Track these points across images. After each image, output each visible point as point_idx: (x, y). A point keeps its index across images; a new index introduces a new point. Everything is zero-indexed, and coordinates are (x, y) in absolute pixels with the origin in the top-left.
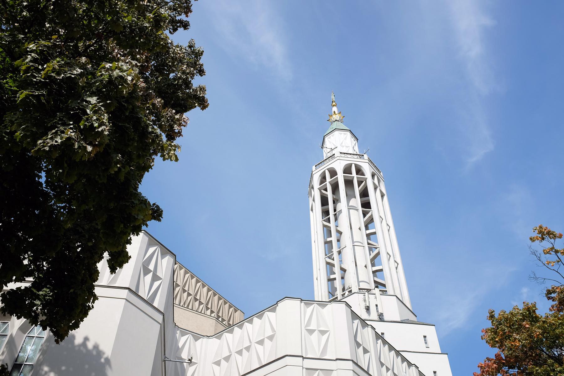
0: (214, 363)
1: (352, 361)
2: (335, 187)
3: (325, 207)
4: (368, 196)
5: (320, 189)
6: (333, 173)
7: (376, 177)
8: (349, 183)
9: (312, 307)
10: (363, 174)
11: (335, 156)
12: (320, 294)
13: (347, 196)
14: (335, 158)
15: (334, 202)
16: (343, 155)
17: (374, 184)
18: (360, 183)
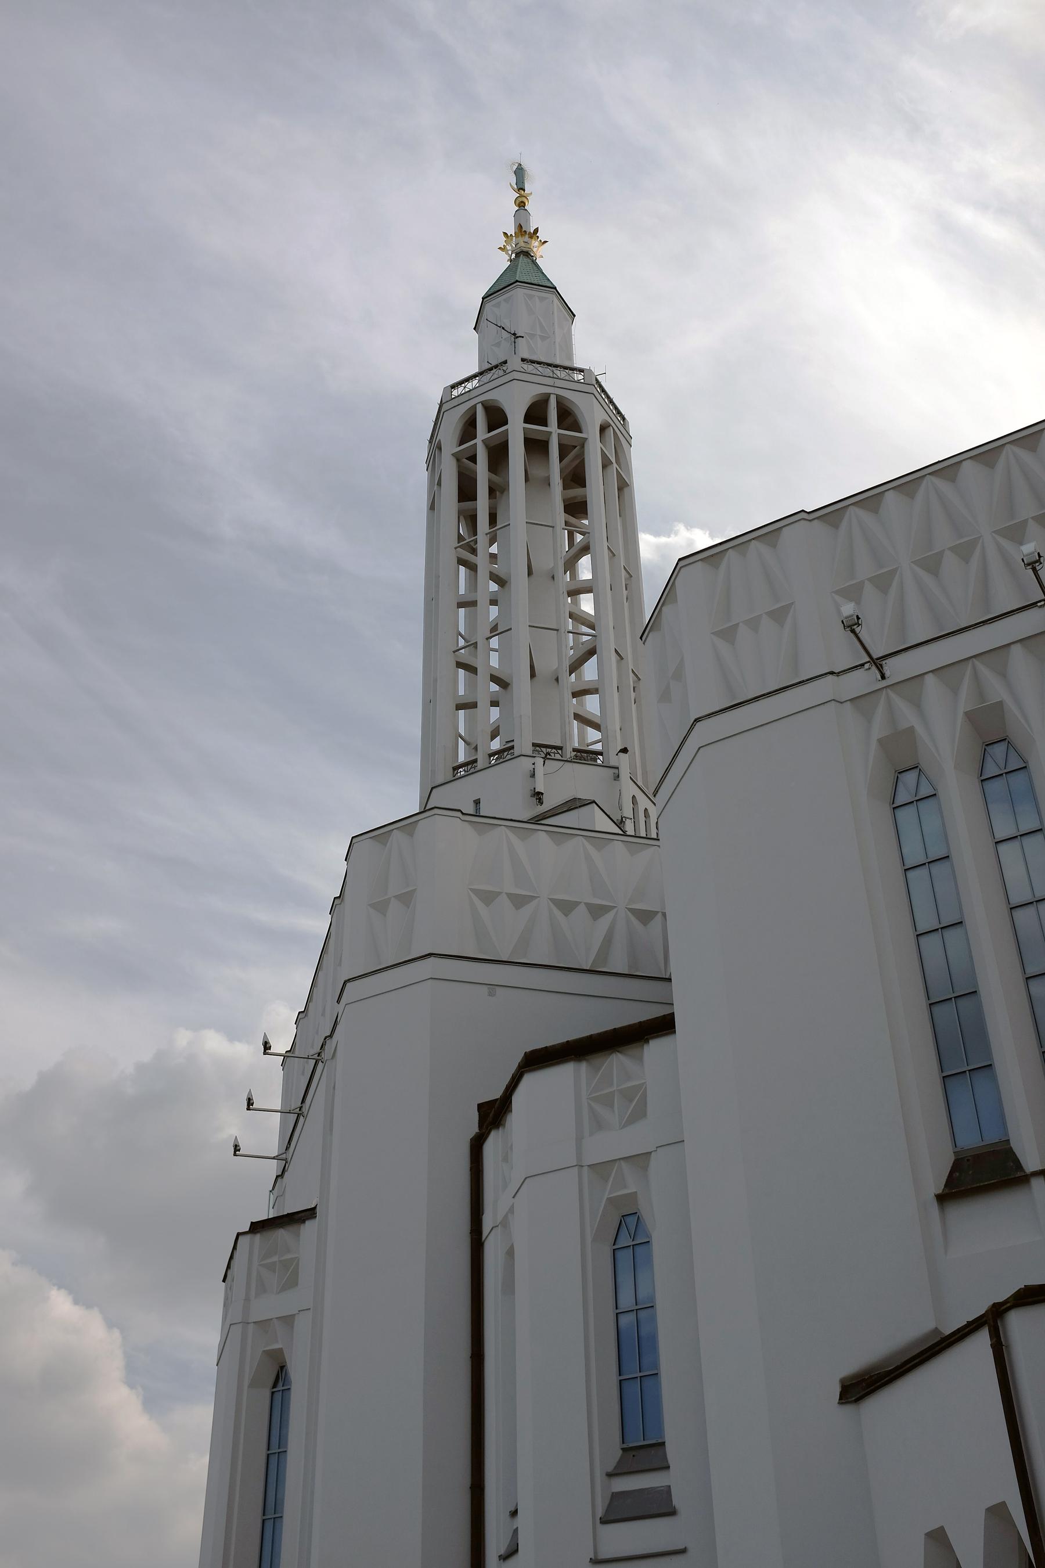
0: (837, 592)
1: (538, 1060)
2: (498, 454)
3: (468, 505)
4: (583, 484)
5: (457, 457)
6: (497, 417)
7: (610, 432)
8: (536, 447)
9: (1004, 452)
10: (576, 427)
11: (509, 367)
12: (559, 383)
13: (527, 480)
14: (505, 373)
15: (492, 491)
16: (529, 368)
17: (604, 456)
18: (564, 450)
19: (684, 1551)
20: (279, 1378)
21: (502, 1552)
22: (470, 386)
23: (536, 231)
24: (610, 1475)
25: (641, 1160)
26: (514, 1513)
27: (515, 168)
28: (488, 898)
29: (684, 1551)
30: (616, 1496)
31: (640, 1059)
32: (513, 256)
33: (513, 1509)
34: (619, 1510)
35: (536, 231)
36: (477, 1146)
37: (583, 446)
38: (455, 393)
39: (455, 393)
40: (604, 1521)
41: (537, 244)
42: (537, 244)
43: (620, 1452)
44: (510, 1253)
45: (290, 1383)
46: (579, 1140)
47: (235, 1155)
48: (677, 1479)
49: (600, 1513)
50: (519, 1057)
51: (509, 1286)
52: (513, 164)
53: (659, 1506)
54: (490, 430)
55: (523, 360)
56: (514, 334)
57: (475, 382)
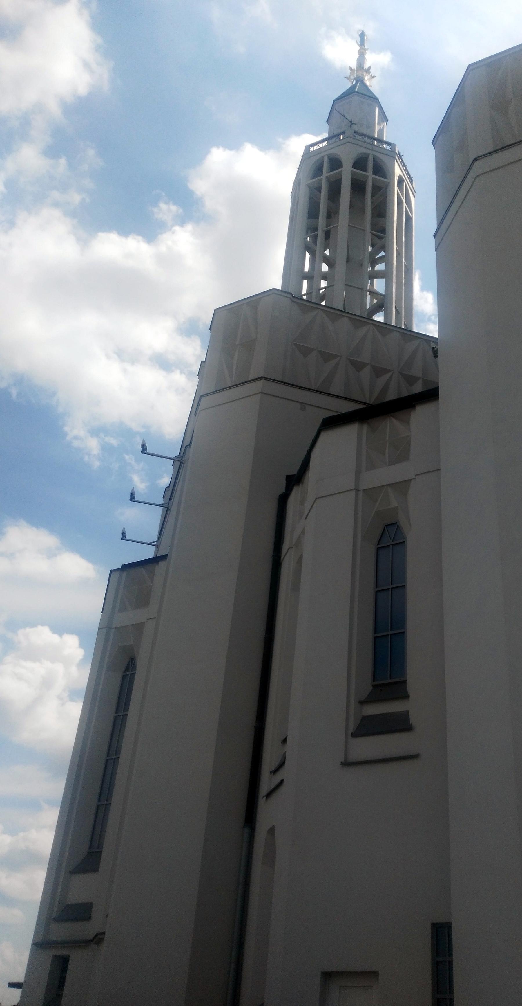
1: (332, 422)
19: (415, 757)
20: (130, 666)
21: (273, 768)
22: (321, 145)
23: (369, 68)
24: (362, 703)
25: (402, 487)
26: (285, 741)
27: (360, 33)
28: (306, 352)
29: (415, 757)
30: (364, 718)
31: (407, 422)
32: (354, 82)
33: (283, 738)
34: (367, 727)
35: (369, 68)
36: (283, 500)
37: (386, 188)
38: (312, 149)
39: (312, 149)
40: (355, 735)
41: (369, 76)
42: (369, 76)
43: (371, 688)
44: (300, 561)
45: (135, 669)
46: (358, 473)
47: (122, 539)
48: (416, 706)
49: (351, 730)
50: (318, 424)
51: (296, 586)
52: (359, 30)
53: (400, 724)
54: (331, 170)
55: (355, 132)
56: (351, 122)
57: (325, 144)
